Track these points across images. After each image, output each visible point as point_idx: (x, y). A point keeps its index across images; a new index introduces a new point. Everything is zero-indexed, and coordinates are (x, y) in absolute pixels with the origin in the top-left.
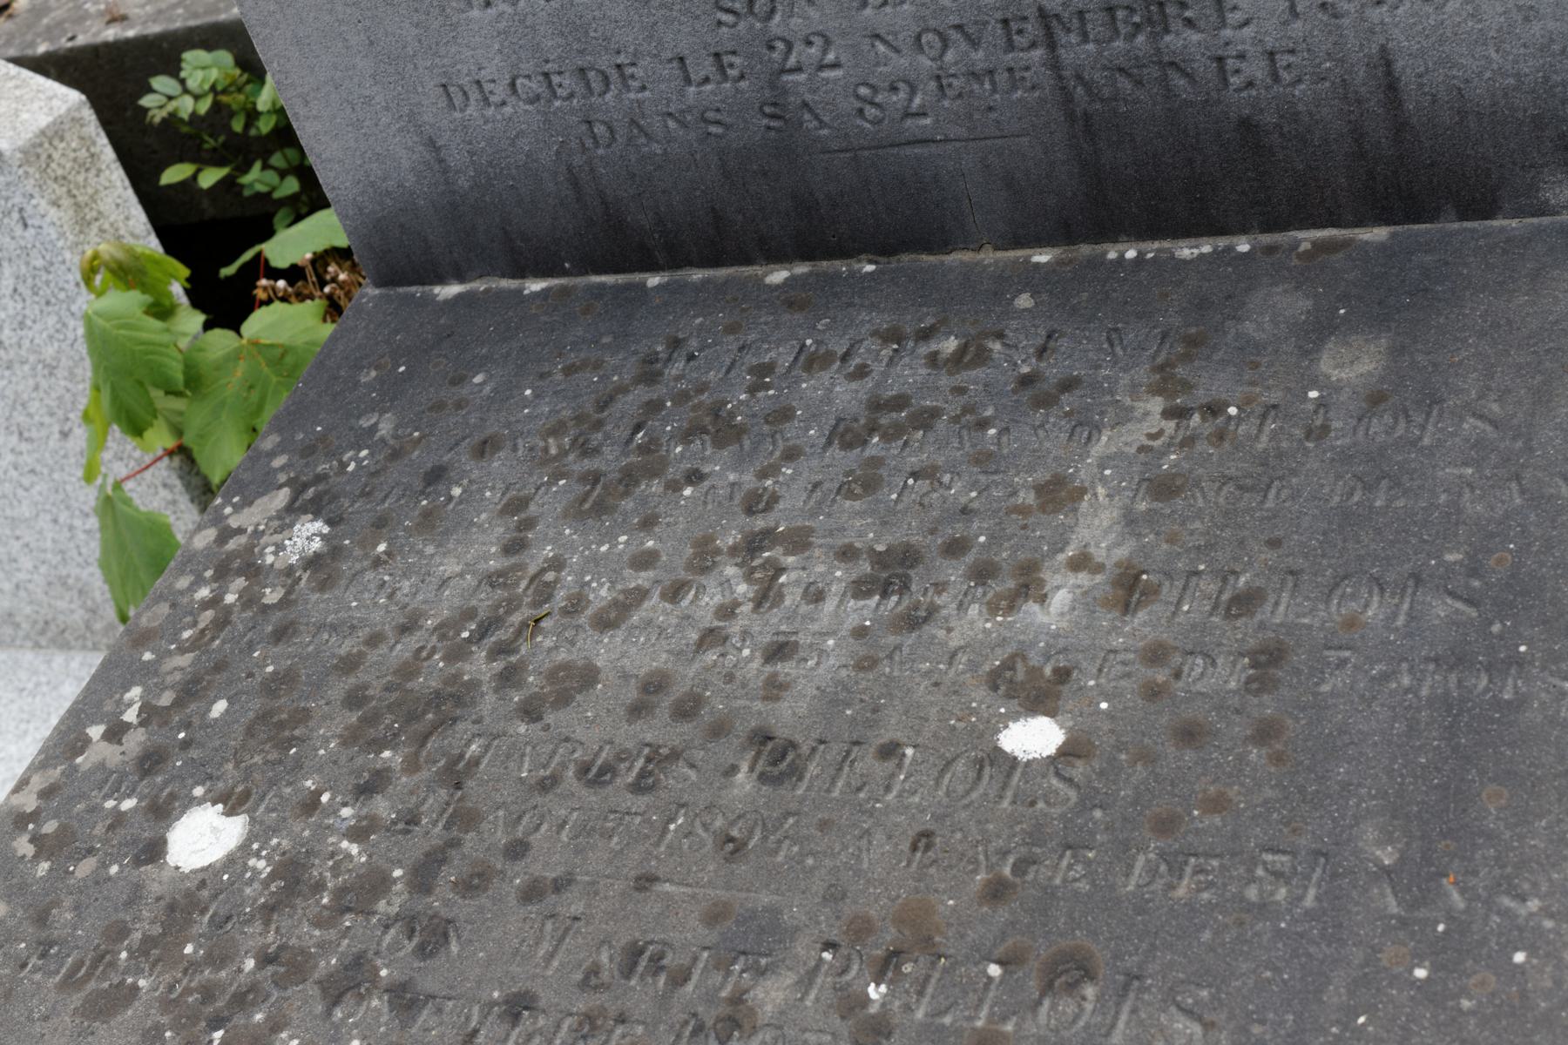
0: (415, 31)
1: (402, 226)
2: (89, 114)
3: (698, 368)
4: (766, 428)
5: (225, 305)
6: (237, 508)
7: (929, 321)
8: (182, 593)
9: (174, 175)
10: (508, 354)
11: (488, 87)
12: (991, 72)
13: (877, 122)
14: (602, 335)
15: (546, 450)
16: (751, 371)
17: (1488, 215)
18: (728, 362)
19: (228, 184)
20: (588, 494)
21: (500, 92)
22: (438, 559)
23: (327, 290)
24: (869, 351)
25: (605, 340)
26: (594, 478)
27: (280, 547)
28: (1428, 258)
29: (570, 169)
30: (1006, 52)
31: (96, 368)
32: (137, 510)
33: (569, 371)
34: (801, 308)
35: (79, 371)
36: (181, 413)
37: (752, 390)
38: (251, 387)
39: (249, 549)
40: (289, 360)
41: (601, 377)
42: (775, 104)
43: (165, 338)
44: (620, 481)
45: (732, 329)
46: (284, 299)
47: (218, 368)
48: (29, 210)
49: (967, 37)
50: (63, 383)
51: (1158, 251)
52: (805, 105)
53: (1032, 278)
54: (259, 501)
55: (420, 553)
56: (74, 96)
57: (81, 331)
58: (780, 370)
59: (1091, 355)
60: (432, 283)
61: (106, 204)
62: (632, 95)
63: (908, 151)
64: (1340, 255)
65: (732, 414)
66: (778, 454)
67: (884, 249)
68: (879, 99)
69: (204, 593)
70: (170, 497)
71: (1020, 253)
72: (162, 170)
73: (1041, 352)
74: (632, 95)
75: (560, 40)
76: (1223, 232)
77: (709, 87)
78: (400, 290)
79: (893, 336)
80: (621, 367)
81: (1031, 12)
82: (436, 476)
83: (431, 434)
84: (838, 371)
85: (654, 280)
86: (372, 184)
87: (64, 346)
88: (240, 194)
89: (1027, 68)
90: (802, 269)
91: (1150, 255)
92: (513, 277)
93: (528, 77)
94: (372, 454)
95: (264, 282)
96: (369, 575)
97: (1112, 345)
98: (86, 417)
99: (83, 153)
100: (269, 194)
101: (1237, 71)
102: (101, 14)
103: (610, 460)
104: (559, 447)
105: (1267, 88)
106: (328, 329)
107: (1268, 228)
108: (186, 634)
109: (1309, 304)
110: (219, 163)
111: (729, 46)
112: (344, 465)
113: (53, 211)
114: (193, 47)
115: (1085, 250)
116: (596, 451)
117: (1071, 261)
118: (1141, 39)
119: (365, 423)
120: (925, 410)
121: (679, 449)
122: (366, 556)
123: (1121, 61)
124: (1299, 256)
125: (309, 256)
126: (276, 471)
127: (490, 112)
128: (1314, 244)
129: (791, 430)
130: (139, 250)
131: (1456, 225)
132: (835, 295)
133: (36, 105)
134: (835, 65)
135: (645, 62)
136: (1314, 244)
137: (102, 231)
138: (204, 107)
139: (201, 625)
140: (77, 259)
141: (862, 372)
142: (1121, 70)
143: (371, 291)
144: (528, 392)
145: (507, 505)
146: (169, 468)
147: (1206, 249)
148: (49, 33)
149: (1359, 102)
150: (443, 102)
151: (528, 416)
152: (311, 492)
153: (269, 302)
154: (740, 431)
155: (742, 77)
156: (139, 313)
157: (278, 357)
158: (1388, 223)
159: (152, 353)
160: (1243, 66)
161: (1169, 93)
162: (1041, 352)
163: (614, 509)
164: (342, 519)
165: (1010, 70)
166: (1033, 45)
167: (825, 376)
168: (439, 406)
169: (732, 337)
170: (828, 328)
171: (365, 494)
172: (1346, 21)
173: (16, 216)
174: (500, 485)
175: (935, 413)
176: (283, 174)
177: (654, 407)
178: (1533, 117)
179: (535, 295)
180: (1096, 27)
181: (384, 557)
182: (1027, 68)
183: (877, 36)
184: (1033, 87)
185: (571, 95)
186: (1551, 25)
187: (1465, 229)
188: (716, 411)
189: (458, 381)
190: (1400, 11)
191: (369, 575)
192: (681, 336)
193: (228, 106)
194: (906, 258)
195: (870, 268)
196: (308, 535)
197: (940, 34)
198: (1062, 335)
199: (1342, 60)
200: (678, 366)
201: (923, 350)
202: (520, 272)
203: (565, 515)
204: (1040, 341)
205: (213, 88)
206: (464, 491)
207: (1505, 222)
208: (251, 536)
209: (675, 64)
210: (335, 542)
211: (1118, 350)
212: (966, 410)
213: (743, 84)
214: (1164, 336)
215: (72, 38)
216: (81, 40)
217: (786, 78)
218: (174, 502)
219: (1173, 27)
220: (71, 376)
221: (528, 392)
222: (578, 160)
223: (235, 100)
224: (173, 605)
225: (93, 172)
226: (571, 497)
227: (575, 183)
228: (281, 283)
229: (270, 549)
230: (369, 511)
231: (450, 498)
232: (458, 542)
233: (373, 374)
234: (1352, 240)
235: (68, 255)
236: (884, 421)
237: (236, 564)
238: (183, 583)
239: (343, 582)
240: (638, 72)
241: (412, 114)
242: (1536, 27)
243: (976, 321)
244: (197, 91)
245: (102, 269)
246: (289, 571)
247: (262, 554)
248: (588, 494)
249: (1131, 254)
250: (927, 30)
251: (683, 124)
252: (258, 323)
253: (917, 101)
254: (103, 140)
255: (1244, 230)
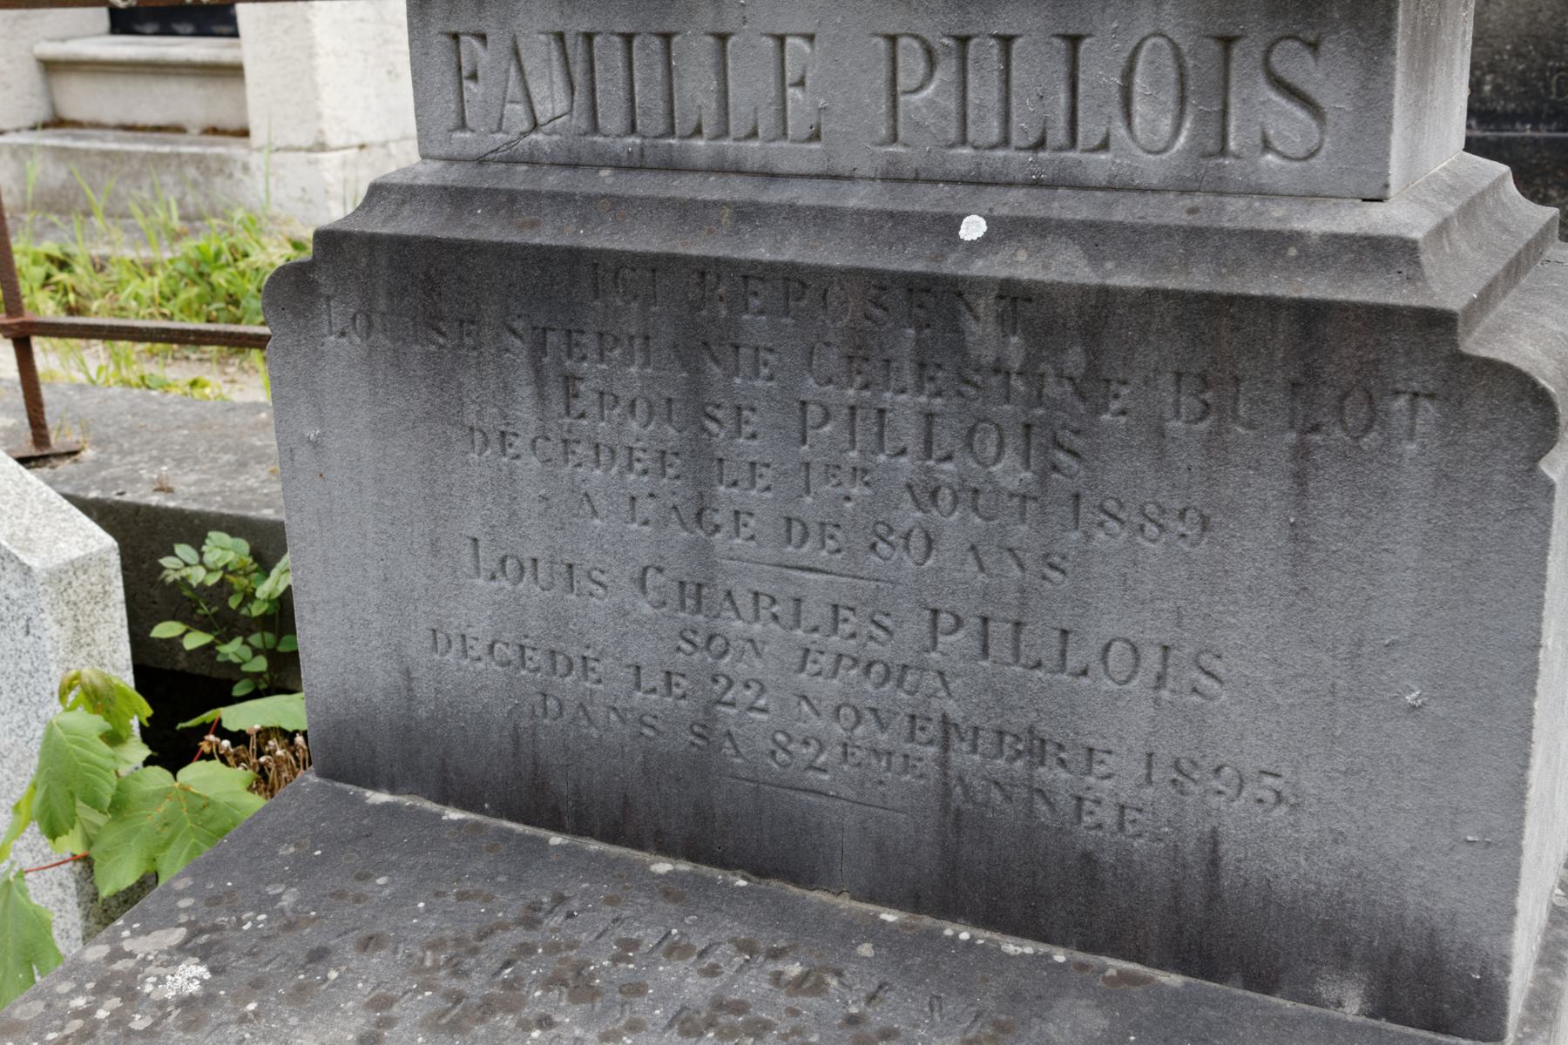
0: (425, 581)
1: (358, 732)
2: (115, 559)
3: (574, 927)
4: (619, 997)
5: (171, 748)
6: (135, 934)
7: (781, 944)
8: (60, 996)
9: (165, 630)
10: (413, 867)
11: (470, 642)
12: (890, 754)
13: (785, 766)
14: (498, 873)
15: (422, 960)
16: (619, 942)
17: (1268, 991)
18: (601, 928)
19: (209, 647)
20: (448, 1010)
21: (479, 649)
22: (298, 1032)
23: (262, 759)
24: (723, 954)
25: (501, 879)
26: (458, 998)
27: (161, 980)
28: (1212, 1013)
29: (516, 728)
30: (906, 741)
31: (40, 770)
32: (29, 902)
33: (462, 896)
34: (676, 901)
35: (24, 766)
36: (98, 828)
37: (616, 960)
38: (166, 825)
39: (133, 974)
40: (208, 812)
41: (488, 911)
42: (704, 727)
43: (109, 763)
44: (479, 1007)
45: (611, 901)
46: (223, 759)
47: (144, 800)
48: (36, 621)
49: (878, 720)
50: (6, 771)
51: (988, 940)
52: (729, 734)
53: (876, 932)
54: (155, 933)
55: (284, 1021)
56: (109, 541)
57: (39, 733)
58: (643, 949)
59: (913, 1013)
60: (366, 787)
61: (101, 635)
62: (588, 684)
63: (803, 796)
64: (1140, 989)
65: (592, 976)
66: (623, 1022)
67: (758, 871)
68: (791, 747)
69: (80, 1002)
70: (61, 896)
71: (871, 908)
72: (160, 621)
73: (871, 998)
74: (588, 684)
75: (543, 623)
76: (1046, 939)
77: (654, 697)
78: (337, 784)
79: (747, 947)
80: (508, 906)
81: (936, 717)
82: (319, 955)
83: (325, 917)
84: (693, 964)
85: (556, 840)
86: (345, 691)
87: (20, 741)
88: (214, 657)
89: (920, 759)
90: (684, 867)
91: (980, 942)
92: (437, 802)
93: (507, 644)
94: (268, 920)
95: (211, 737)
96: (233, 1029)
97: (932, 1010)
98: (16, 809)
99: (99, 588)
100: (239, 665)
101: (1091, 813)
102: (152, 481)
103: (476, 986)
104: (435, 961)
105: (1112, 834)
106: (256, 802)
107: (1083, 948)
108: (51, 1036)
109: (1105, 1023)
110: (206, 629)
111: (681, 669)
112: (240, 923)
113: (56, 627)
114: (219, 529)
115: (927, 921)
116: (466, 974)
117: (913, 927)
118: (1019, 763)
119: (272, 890)
120: (759, 1021)
121: (538, 993)
122: (235, 1010)
123: (999, 777)
124: (1105, 979)
125: (257, 727)
126: (180, 910)
127: (465, 662)
128: (1120, 972)
129: (640, 1004)
130: (115, 681)
131: (1240, 992)
132: (707, 897)
133: (74, 539)
134: (763, 710)
135: (608, 661)
136: (1120, 972)
137: (90, 655)
138: (212, 580)
139: (67, 1032)
140: (60, 673)
141: (713, 971)
142: (996, 783)
143: (309, 777)
144: (421, 905)
145: (373, 1000)
146: (71, 871)
147: (1029, 950)
148: (103, 484)
149: (1184, 866)
150: (428, 644)
151: (415, 926)
152: (204, 938)
153: (209, 757)
154: (595, 993)
155: (684, 696)
156: (95, 736)
157: (201, 807)
158: (1184, 973)
159: (100, 776)
160: (1097, 810)
161: (1031, 813)
162: (871, 998)
163: (468, 1030)
164: (224, 971)
165: (906, 756)
166: (930, 742)
167: (681, 966)
168: (340, 895)
169: (609, 908)
170: (694, 924)
171: (251, 954)
172: (1189, 799)
173: (22, 622)
174: (373, 980)
175: (767, 1026)
176: (256, 652)
177: (527, 949)
178: (1324, 921)
179: (452, 823)
180: (986, 741)
181: (251, 1016)
182: (920, 759)
183: (805, 698)
184: (921, 776)
185: (537, 669)
186: (1354, 852)
187: (1248, 998)
188: (579, 969)
189: (364, 877)
190: (1235, 804)
191: (233, 1029)
192: (566, 894)
193: (232, 584)
194: (775, 884)
195: (742, 883)
196: (190, 976)
197: (857, 711)
198: (891, 989)
199: (1179, 829)
200: (557, 920)
201: (771, 967)
202: (445, 799)
203: (422, 1024)
204: (872, 988)
205: (225, 568)
206: (340, 977)
207: (1282, 1001)
208: (138, 963)
209: (632, 670)
210: (212, 990)
211: (936, 1015)
212: (796, 1031)
213: (683, 703)
214: (978, 1016)
215: (121, 494)
216: (128, 498)
217: (719, 708)
218: (63, 901)
219: (1048, 762)
220: (16, 768)
221: (421, 905)
222: (525, 723)
223: (239, 582)
224: (48, 1006)
225: (101, 605)
226: (433, 1009)
227: (516, 739)
228: (226, 743)
229: (152, 979)
230: (250, 970)
231: (325, 979)
232: (321, 1021)
233: (292, 850)
234: (1151, 979)
235: (53, 667)
236: (722, 1020)
237: (117, 985)
238: (64, 987)
239: (207, 1028)
240: (599, 667)
241: (399, 645)
242: (1342, 851)
243: (821, 955)
244: (211, 566)
245: (78, 688)
246: (163, 1004)
247: (143, 982)
248: (448, 1010)
249: (964, 936)
250: (847, 705)
251: (623, 720)
252: (196, 774)
253: (822, 758)
254: (119, 583)
255: (1064, 944)
